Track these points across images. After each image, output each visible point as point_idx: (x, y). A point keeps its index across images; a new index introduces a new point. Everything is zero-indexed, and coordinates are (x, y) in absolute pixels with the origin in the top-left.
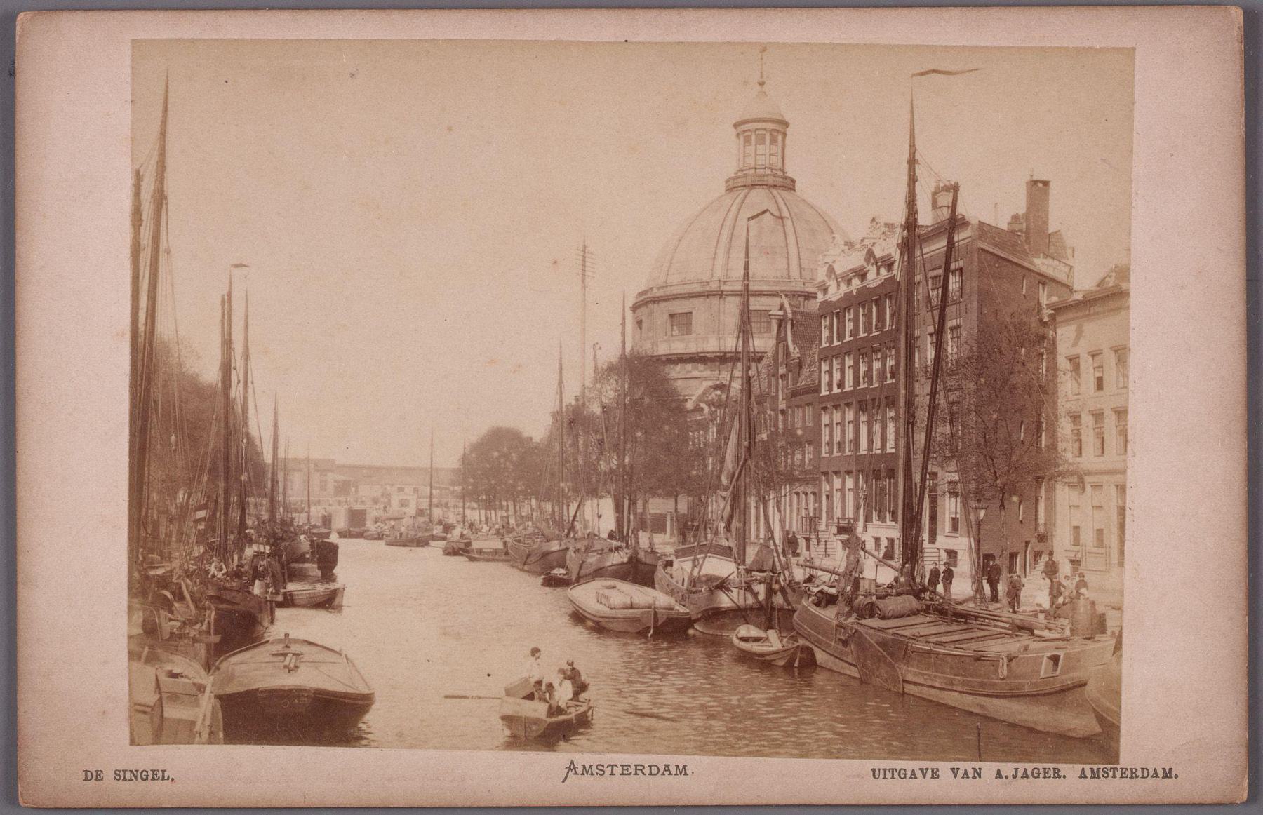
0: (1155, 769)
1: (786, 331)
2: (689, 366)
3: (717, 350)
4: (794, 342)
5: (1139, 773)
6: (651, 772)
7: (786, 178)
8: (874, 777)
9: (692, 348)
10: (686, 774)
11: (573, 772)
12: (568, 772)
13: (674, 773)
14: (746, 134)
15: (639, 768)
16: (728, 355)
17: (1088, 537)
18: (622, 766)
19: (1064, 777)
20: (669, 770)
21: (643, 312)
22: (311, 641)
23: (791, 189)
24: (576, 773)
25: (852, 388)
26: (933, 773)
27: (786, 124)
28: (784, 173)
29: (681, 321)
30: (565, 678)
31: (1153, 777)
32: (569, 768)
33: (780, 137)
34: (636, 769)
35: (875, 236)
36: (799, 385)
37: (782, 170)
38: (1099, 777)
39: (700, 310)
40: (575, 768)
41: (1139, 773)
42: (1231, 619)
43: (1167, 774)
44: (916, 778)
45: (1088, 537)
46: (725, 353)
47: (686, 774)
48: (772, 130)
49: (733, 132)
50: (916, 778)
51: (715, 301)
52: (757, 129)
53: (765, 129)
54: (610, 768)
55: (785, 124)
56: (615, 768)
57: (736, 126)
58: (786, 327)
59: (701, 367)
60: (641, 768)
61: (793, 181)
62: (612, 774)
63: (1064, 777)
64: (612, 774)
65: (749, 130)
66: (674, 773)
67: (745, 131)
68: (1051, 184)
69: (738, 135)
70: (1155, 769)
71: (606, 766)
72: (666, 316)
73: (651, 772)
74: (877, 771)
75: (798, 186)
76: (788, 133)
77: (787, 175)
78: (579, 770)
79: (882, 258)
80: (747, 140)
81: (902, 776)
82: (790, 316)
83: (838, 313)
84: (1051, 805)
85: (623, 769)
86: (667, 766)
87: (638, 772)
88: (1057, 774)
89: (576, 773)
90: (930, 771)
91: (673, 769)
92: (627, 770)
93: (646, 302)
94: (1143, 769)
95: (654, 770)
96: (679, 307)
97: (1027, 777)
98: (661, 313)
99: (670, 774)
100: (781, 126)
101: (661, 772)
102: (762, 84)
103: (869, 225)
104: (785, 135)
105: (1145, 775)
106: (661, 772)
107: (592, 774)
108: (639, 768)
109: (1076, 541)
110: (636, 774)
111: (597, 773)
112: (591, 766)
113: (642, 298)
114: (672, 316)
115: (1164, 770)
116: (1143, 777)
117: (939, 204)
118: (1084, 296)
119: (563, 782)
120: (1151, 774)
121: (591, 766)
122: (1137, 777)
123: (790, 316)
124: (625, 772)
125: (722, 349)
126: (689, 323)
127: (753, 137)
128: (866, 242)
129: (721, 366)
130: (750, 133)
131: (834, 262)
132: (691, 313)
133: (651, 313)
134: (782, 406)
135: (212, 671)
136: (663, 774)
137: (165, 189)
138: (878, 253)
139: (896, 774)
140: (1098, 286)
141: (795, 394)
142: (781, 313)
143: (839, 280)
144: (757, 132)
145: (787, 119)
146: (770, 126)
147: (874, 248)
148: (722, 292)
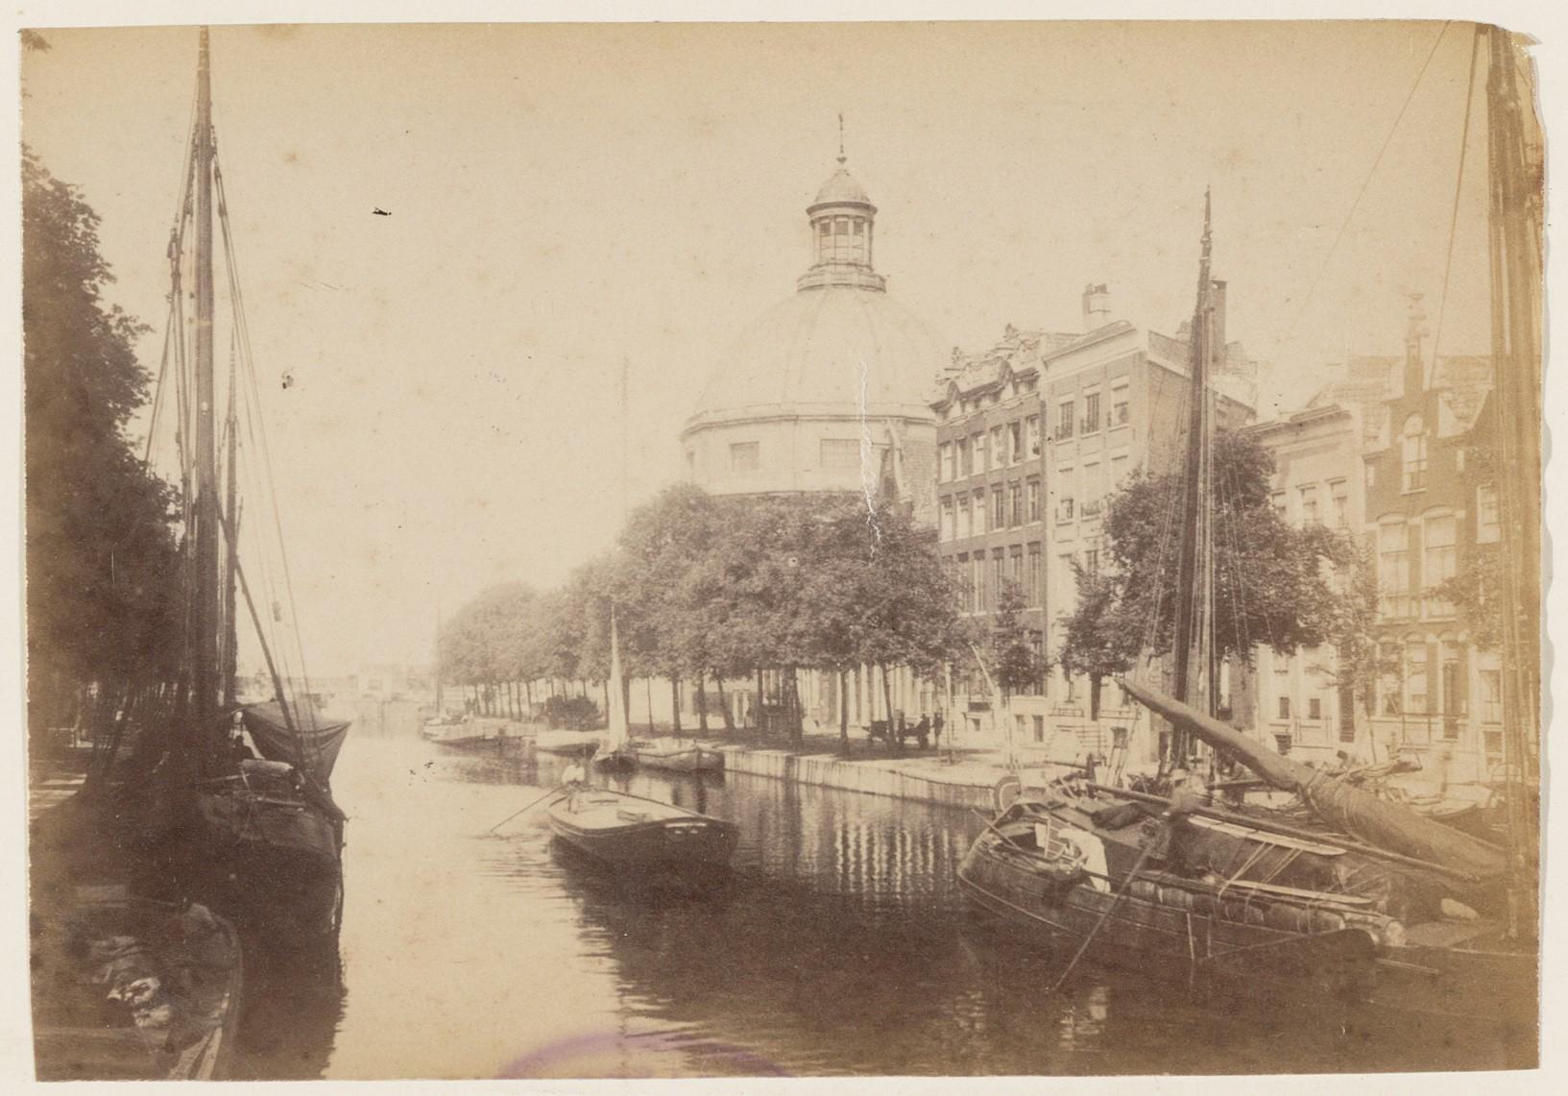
7: (874, 276)
14: (823, 222)
17: (1300, 708)
22: (249, 589)
23: (881, 289)
25: (983, 533)
27: (875, 210)
28: (871, 270)
30: (627, 1017)
33: (866, 227)
35: (1011, 346)
37: (869, 267)
39: (769, 438)
42: (665, 491)
45: (1300, 708)
49: (808, 219)
51: (787, 427)
52: (836, 216)
53: (847, 216)
55: (868, 208)
57: (810, 211)
58: (892, 459)
67: (821, 218)
68: (1228, 286)
69: (812, 223)
75: (888, 285)
77: (875, 272)
79: (1022, 372)
80: (825, 229)
82: (898, 444)
93: (699, 428)
98: (720, 439)
104: (871, 224)
109: (1285, 713)
113: (694, 424)
114: (734, 446)
117: (1092, 309)
118: (1291, 419)
127: (833, 225)
128: (1001, 353)
130: (827, 221)
132: (757, 443)
140: (1308, 406)
142: (887, 441)
144: (839, 220)
145: (874, 203)
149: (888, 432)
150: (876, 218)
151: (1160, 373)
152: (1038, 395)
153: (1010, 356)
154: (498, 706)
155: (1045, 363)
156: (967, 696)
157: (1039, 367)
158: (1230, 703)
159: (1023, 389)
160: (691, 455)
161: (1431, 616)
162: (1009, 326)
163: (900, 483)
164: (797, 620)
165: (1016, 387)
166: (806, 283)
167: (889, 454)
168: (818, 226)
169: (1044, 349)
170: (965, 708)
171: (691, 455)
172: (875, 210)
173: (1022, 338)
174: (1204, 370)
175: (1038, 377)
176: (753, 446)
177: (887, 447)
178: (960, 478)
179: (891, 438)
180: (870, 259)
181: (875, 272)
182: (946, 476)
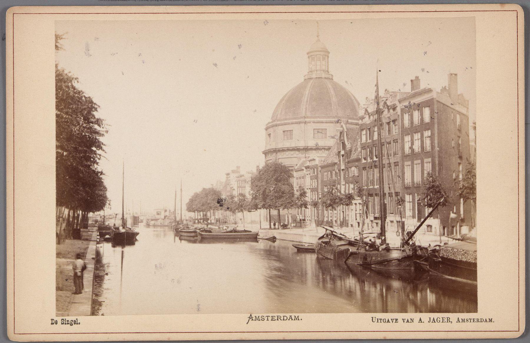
0: (486, 319)
1: (344, 137)
2: (292, 152)
3: (304, 145)
4: (348, 141)
5: (480, 320)
6: (284, 319)
8: (373, 321)
9: (293, 145)
10: (299, 320)
11: (251, 319)
12: (249, 319)
13: (293, 319)
15: (279, 317)
16: (309, 148)
18: (272, 316)
19: (494, 322)
20: (291, 318)
21: (271, 131)
24: (253, 320)
26: (396, 321)
27: (329, 53)
28: (328, 72)
29: (288, 134)
31: (387, 322)
32: (250, 317)
33: (326, 58)
34: (278, 318)
36: (351, 158)
38: (464, 322)
40: (252, 317)
41: (480, 320)
43: (491, 320)
44: (389, 322)
46: (308, 147)
47: (299, 320)
48: (324, 55)
49: (307, 56)
50: (389, 322)
53: (320, 55)
54: (267, 317)
56: (269, 317)
57: (308, 54)
59: (297, 152)
60: (280, 317)
61: (332, 76)
62: (268, 320)
63: (424, 322)
64: (268, 320)
65: (313, 55)
66: (293, 319)
70: (486, 319)
71: (265, 317)
72: (282, 132)
73: (284, 319)
74: (374, 319)
76: (329, 56)
77: (330, 73)
78: (254, 319)
81: (384, 322)
82: (345, 130)
83: (369, 129)
84: (220, 340)
85: (272, 318)
86: (291, 316)
87: (279, 319)
88: (448, 319)
89: (253, 320)
90: (395, 320)
91: (293, 318)
92: (274, 318)
94: (481, 319)
95: (285, 318)
96: (287, 128)
97: (435, 322)
98: (280, 129)
99: (292, 320)
100: (326, 53)
101: (288, 319)
102: (318, 36)
103: (384, 92)
104: (328, 57)
105: (482, 321)
106: (288, 319)
107: (259, 320)
108: (279, 317)
110: (278, 320)
111: (261, 320)
112: (259, 317)
115: (462, 319)
116: (481, 322)
119: (247, 323)
120: (484, 321)
121: (259, 317)
122: (479, 322)
123: (345, 130)
124: (273, 319)
125: (306, 145)
126: (291, 135)
129: (306, 152)
130: (314, 56)
131: (367, 107)
133: (274, 131)
134: (343, 167)
135: (270, 280)
136: (289, 320)
137: (424, 117)
138: (389, 103)
139: (382, 321)
141: (348, 162)
142: (342, 129)
143: (370, 115)
144: (317, 56)
146: (322, 53)
147: (387, 102)
148: (306, 121)
149: (342, 126)
150: (330, 55)
151: (442, 105)
152: (397, 113)
153: (387, 100)
154: (417, 169)
155: (399, 102)
156: (373, 215)
157: (397, 103)
158: (464, 216)
159: (391, 111)
160: (269, 135)
161: (414, 217)
162: (386, 90)
163: (346, 143)
164: (221, 211)
165: (389, 110)
166: (306, 77)
167: (342, 133)
168: (310, 58)
169: (398, 97)
170: (372, 219)
171: (269, 135)
172: (329, 53)
173: (391, 94)
174: (424, 111)
175: (397, 107)
176: (291, 131)
177: (342, 131)
178: (369, 141)
179: (343, 128)
180: (328, 68)
181: (330, 73)
182: (364, 140)
